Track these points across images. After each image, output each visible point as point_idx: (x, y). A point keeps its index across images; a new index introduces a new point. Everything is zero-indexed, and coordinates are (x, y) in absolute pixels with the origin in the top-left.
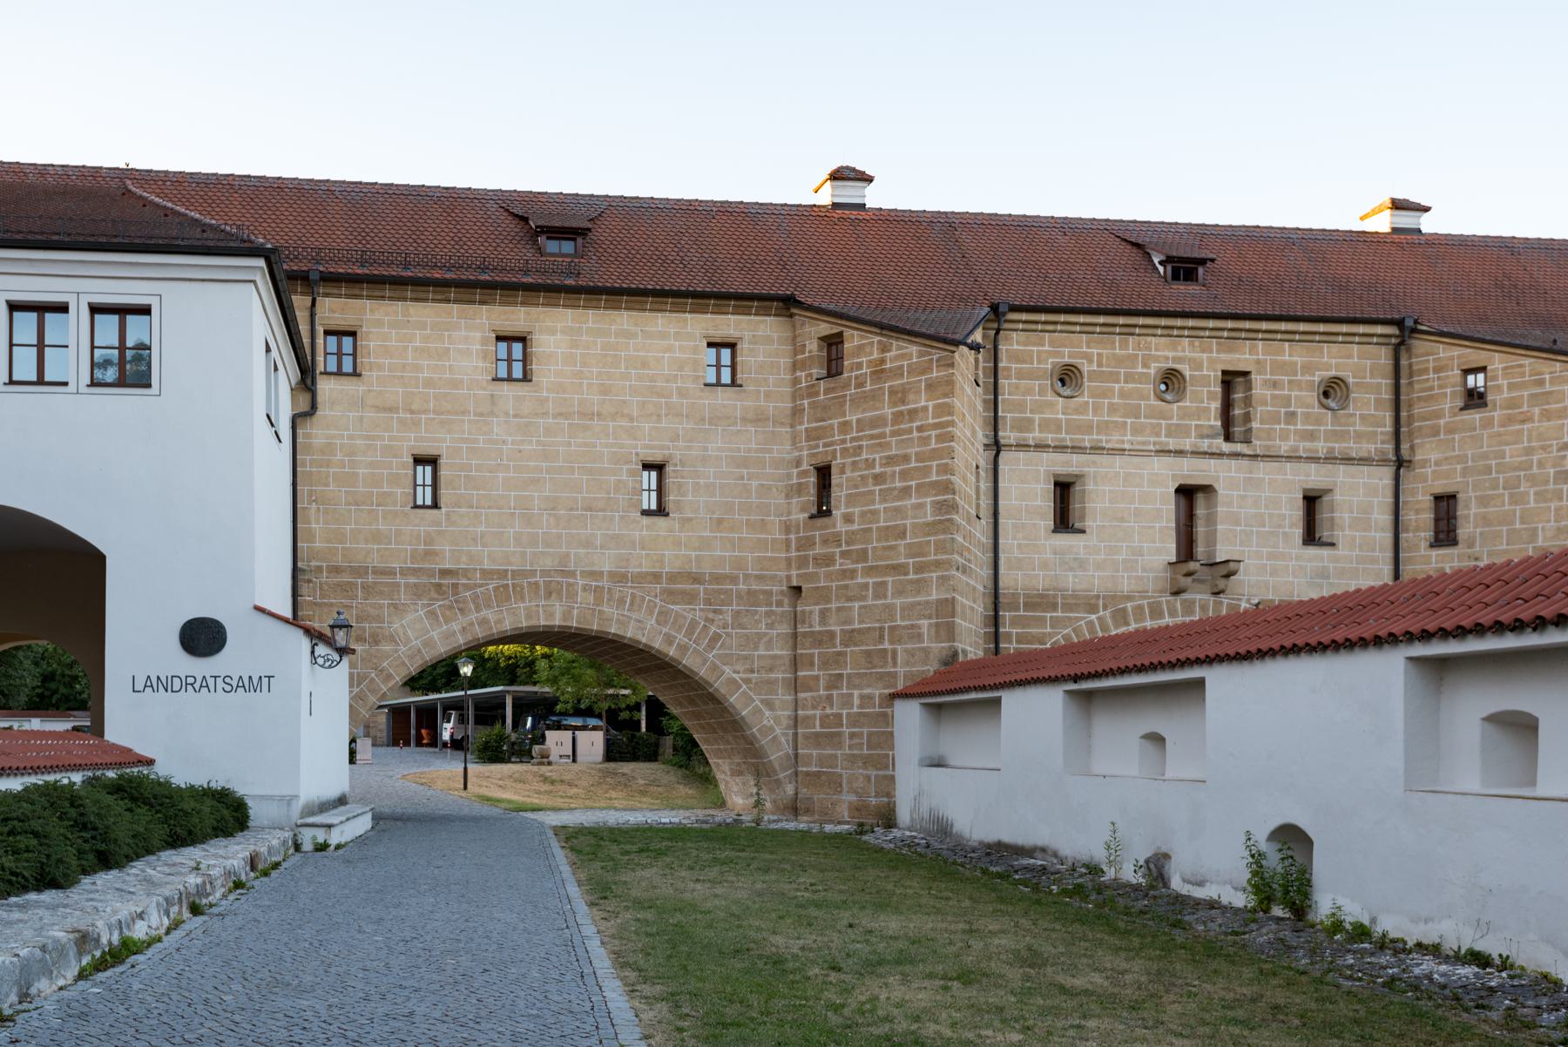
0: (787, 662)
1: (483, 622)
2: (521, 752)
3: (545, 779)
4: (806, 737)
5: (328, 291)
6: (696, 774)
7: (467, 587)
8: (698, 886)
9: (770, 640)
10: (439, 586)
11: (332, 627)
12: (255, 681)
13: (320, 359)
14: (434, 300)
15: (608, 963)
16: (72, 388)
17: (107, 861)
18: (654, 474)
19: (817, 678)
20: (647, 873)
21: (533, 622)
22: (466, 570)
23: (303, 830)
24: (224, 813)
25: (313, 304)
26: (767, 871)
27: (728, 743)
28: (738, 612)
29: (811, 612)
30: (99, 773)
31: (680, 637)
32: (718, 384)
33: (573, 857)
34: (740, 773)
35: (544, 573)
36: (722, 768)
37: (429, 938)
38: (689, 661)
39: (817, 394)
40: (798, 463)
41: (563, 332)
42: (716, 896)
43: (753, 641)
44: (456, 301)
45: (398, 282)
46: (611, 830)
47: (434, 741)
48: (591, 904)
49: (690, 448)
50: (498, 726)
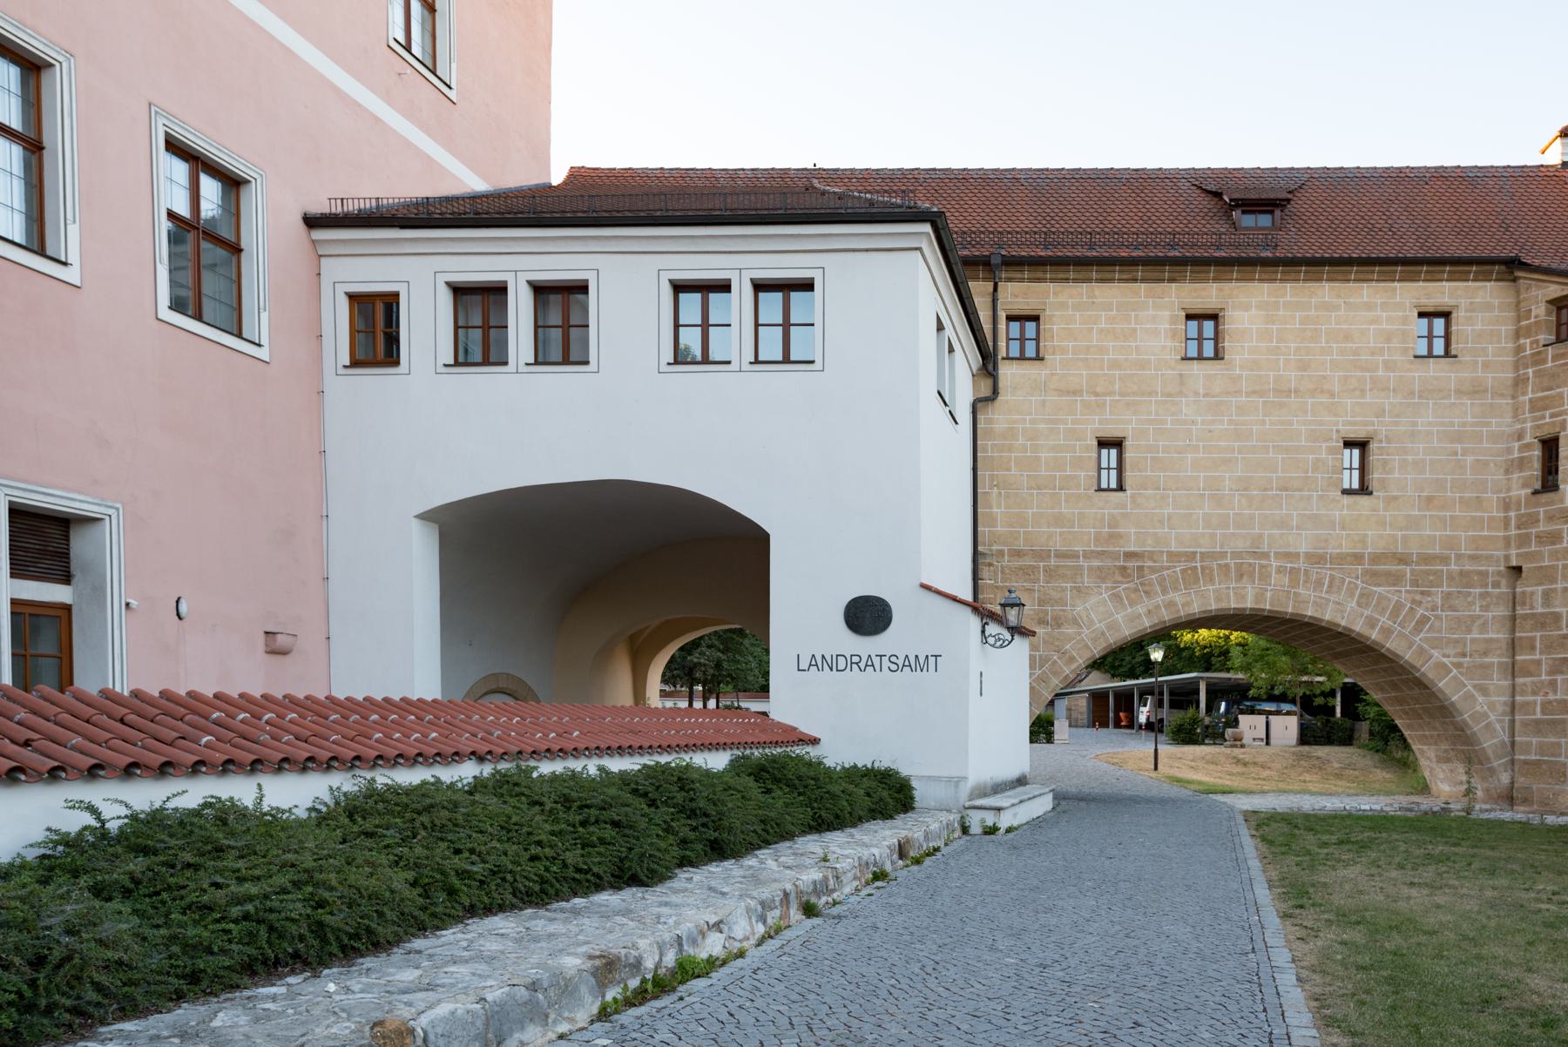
0: (1504, 646)
1: (1170, 605)
2: (1214, 735)
3: (1238, 761)
4: (1525, 724)
5: (1010, 275)
6: (1393, 759)
7: (1153, 570)
8: (1414, 892)
9: (1485, 624)
10: (1124, 568)
11: (1003, 606)
12: (922, 660)
13: (1002, 344)
14: (1120, 280)
15: (1307, 1018)
16: (734, 366)
17: (719, 850)
18: (1356, 452)
19: (1539, 662)
20: (1351, 872)
21: (1224, 605)
22: (1152, 553)
23: (970, 812)
24: (886, 794)
25: (995, 289)
26: (1492, 873)
27: (1435, 729)
28: (1449, 594)
29: (1532, 593)
30: (748, 752)
31: (1384, 620)
32: (1430, 355)
33: (1264, 848)
34: (1448, 760)
35: (1235, 555)
36: (1427, 755)
37: (1073, 962)
38: (1392, 645)
39: (1544, 361)
40: (1520, 436)
41: (1259, 307)
42: (1438, 907)
43: (1466, 624)
44: (1143, 280)
45: (1082, 263)
46: (1307, 816)
47: (1131, 724)
48: (1285, 916)
49: (1397, 424)
50: (1191, 711)
